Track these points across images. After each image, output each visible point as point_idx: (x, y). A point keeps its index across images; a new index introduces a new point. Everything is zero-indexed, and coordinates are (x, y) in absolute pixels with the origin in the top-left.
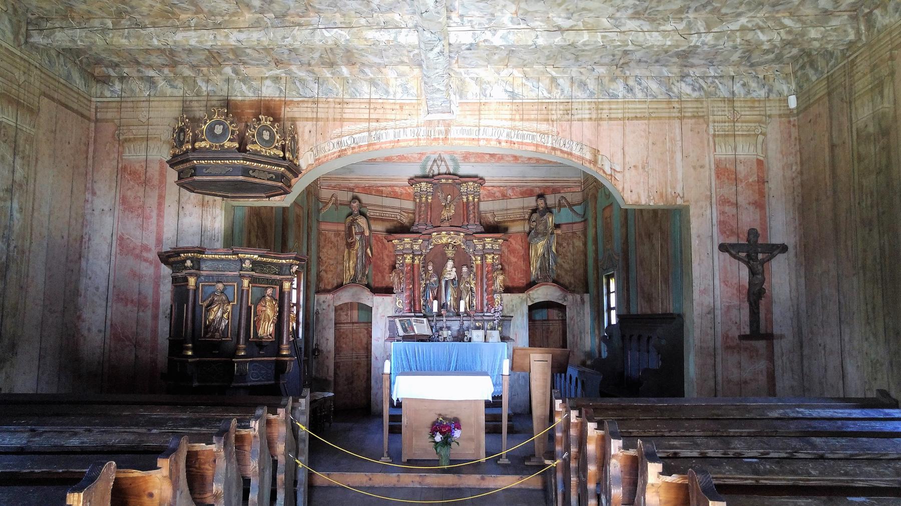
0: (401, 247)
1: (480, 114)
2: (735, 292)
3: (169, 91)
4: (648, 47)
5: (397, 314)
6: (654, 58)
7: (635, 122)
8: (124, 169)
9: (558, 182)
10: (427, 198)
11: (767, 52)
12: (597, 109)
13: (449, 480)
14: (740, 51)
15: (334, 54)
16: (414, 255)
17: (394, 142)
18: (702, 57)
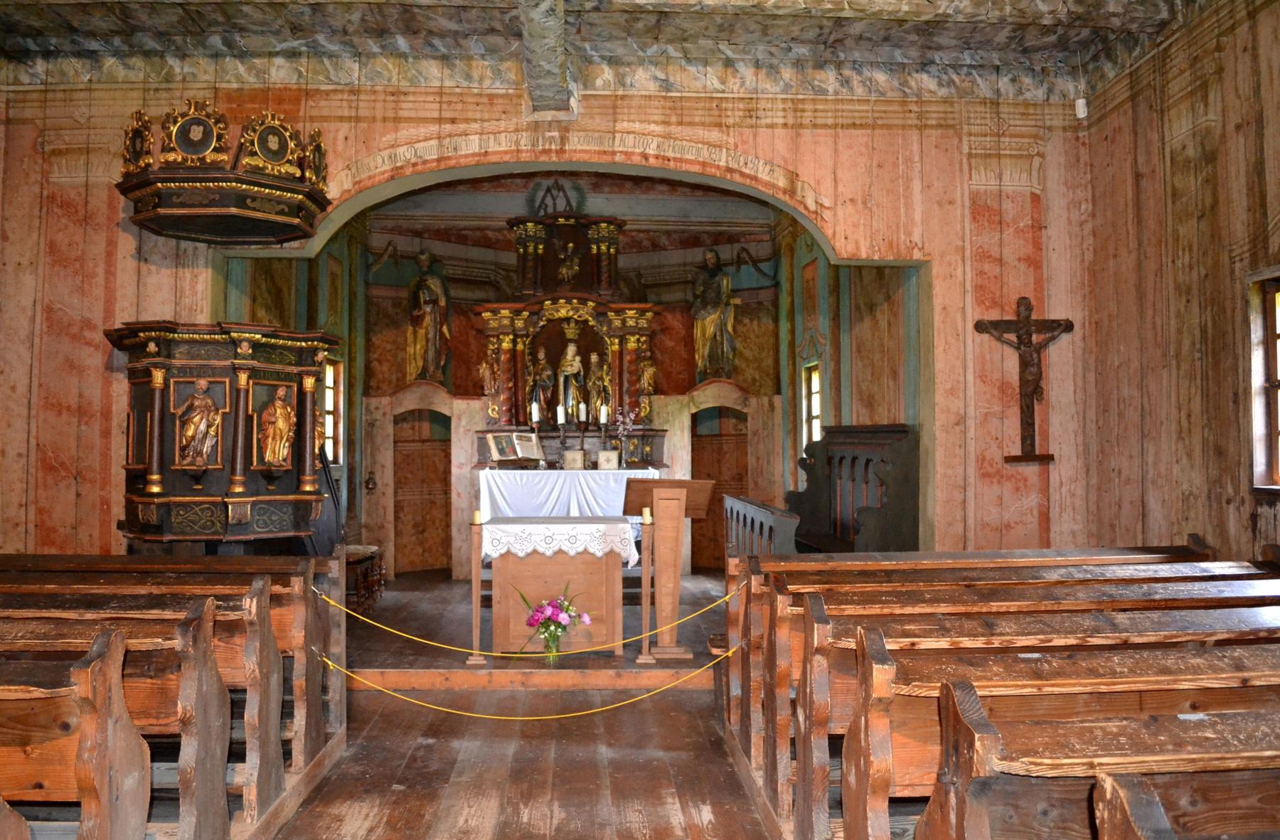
0: (493, 324)
1: (615, 113)
2: (996, 391)
3: (121, 73)
4: (874, 14)
5: (490, 428)
6: (882, 33)
7: (854, 132)
8: (52, 198)
9: (737, 225)
10: (536, 248)
11: (1047, 30)
12: (796, 110)
13: (568, 678)
14: (1009, 28)
15: (383, 16)
16: (516, 336)
17: (479, 155)
18: (952, 34)
